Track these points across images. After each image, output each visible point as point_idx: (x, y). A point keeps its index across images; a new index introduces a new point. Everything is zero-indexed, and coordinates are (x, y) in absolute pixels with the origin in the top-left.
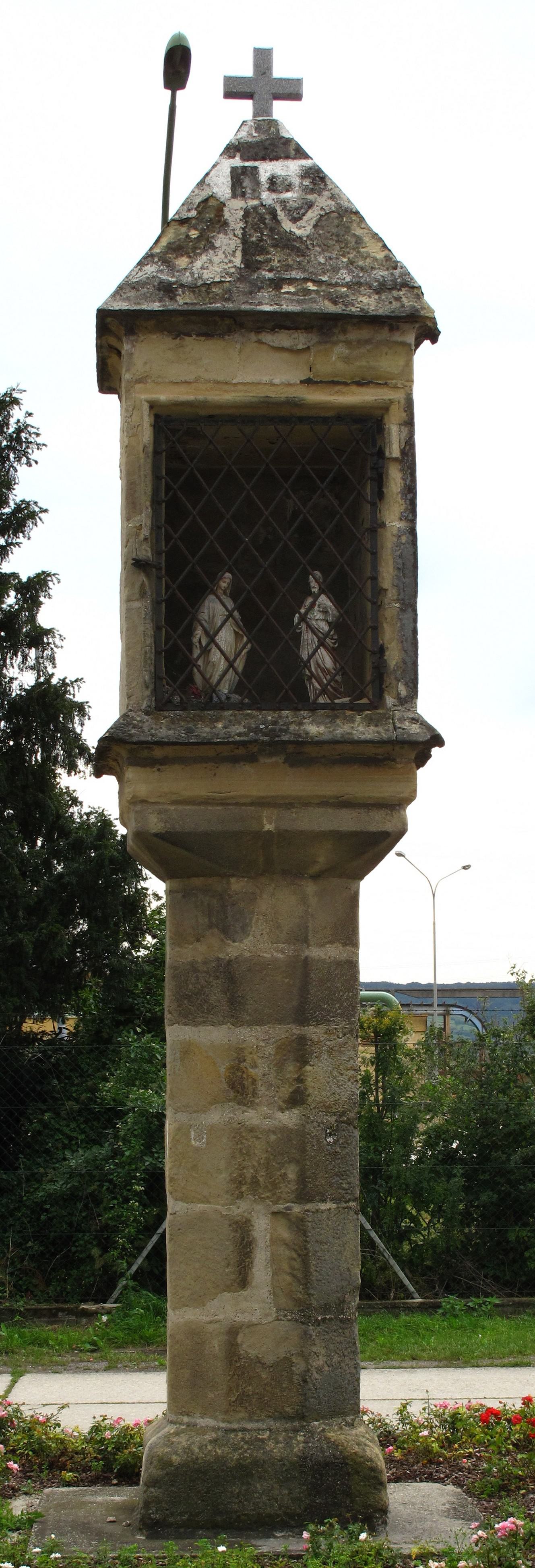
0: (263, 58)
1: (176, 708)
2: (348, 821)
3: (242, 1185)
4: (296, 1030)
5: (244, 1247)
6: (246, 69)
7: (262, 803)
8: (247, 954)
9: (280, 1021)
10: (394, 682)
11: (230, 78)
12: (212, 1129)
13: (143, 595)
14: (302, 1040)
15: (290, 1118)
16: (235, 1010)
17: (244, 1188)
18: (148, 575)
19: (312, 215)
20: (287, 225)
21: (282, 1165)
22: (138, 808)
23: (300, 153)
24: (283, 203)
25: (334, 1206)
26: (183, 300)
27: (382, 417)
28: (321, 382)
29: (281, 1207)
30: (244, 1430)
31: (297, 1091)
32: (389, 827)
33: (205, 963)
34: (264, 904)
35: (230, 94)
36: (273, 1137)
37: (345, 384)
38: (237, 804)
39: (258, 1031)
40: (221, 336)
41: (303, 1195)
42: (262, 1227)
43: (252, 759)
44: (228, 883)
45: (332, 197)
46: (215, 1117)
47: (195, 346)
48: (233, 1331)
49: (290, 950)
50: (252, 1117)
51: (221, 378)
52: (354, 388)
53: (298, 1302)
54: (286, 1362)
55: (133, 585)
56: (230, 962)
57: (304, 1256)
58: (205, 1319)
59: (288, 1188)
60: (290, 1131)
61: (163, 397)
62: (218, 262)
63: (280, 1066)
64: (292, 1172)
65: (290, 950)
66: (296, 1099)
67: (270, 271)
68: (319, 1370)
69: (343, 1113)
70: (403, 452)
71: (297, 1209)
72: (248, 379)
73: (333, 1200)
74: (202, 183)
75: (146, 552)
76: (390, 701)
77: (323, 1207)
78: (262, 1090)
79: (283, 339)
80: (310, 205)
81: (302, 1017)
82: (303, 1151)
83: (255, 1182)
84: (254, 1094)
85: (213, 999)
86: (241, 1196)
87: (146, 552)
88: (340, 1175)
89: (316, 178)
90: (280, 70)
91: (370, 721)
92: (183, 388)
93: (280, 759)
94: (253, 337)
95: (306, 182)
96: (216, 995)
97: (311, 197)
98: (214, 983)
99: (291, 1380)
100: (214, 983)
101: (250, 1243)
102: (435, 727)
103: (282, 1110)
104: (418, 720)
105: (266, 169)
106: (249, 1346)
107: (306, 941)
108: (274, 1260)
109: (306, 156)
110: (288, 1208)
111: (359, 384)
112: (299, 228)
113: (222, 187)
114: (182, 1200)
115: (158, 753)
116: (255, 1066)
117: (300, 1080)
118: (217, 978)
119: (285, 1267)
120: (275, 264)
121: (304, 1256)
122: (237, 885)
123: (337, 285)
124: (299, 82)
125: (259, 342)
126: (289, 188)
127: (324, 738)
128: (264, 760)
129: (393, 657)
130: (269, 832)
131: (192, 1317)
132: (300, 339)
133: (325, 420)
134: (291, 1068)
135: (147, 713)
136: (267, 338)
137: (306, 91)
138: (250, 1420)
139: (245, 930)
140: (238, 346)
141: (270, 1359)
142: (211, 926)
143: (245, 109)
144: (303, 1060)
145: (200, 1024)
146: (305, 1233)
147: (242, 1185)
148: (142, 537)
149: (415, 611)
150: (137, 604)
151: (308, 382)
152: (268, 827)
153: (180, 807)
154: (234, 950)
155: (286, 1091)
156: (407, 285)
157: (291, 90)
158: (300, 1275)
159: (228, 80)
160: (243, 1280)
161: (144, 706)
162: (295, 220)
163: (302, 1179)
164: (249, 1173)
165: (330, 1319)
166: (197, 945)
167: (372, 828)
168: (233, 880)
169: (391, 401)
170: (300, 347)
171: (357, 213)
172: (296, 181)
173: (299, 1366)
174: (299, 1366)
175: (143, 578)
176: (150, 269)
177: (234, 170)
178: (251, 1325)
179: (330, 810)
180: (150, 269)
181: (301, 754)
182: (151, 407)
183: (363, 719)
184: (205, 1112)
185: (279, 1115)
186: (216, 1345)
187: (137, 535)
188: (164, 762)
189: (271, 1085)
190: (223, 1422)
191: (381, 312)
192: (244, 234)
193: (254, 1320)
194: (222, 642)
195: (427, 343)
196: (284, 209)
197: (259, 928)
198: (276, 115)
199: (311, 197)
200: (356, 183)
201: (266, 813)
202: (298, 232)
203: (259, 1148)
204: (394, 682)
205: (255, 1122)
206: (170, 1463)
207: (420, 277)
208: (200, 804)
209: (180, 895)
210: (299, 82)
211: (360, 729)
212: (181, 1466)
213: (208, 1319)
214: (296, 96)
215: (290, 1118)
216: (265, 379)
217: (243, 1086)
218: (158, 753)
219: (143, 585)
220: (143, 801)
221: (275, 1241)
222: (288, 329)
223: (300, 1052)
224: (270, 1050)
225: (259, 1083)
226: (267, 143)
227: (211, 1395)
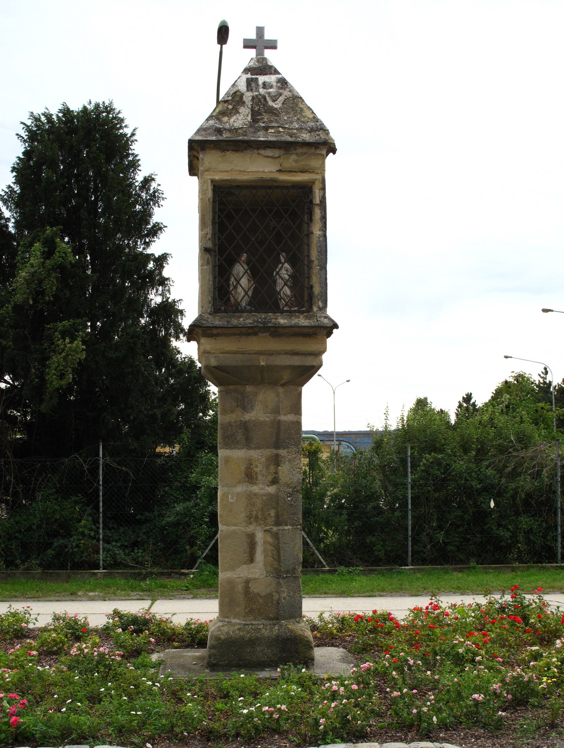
0: (260, 31)
1: (222, 312)
2: (297, 361)
3: (251, 519)
4: (275, 451)
5: (252, 545)
7: (259, 353)
8: (253, 419)
9: (267, 448)
10: (317, 301)
12: (238, 494)
13: (208, 263)
14: (277, 456)
15: (272, 490)
16: (248, 443)
20: (271, 103)
21: (268, 510)
22: (206, 355)
23: (276, 72)
24: (269, 93)
25: (291, 527)
26: (226, 136)
27: (312, 186)
30: (252, 624)
31: (275, 478)
32: (315, 363)
34: (260, 397)
35: (245, 47)
36: (264, 498)
37: (296, 172)
38: (249, 354)
39: (258, 452)
40: (242, 151)
41: (278, 523)
42: (260, 536)
43: (255, 334)
44: (245, 388)
45: (290, 91)
46: (240, 489)
48: (247, 582)
49: (272, 417)
50: (255, 489)
51: (242, 169)
52: (300, 174)
53: (275, 569)
54: (271, 594)
55: (204, 259)
56: (246, 422)
58: (235, 576)
62: (240, 119)
63: (268, 467)
64: (273, 513)
66: (275, 481)
68: (285, 599)
69: (295, 487)
70: (321, 201)
71: (275, 529)
72: (254, 170)
73: (291, 525)
74: (234, 85)
75: (210, 245)
76: (315, 309)
77: (286, 528)
78: (260, 477)
79: (269, 152)
80: (281, 95)
81: (277, 446)
82: (278, 504)
83: (257, 517)
84: (256, 479)
86: (251, 523)
87: (210, 245)
88: (293, 514)
89: (283, 83)
90: (268, 36)
91: (306, 318)
92: (225, 174)
93: (268, 334)
94: (256, 151)
95: (279, 85)
96: (240, 436)
97: (281, 91)
98: (239, 431)
99: (272, 603)
101: (255, 544)
103: (268, 486)
104: (327, 317)
105: (262, 79)
106: (255, 588)
107: (279, 413)
108: (265, 551)
109: (279, 73)
110: (271, 528)
111: (302, 172)
112: (276, 104)
114: (225, 525)
115: (215, 331)
116: (257, 467)
117: (276, 473)
118: (241, 429)
119: (270, 554)
123: (292, 129)
125: (259, 154)
126: (271, 87)
128: (261, 335)
131: (230, 576)
132: (276, 153)
133: (287, 187)
134: (272, 468)
135: (210, 314)
137: (279, 45)
138: (255, 620)
139: (252, 408)
141: (263, 594)
142: (237, 407)
143: (252, 53)
144: (278, 464)
146: (278, 539)
147: (251, 519)
150: (206, 267)
151: (280, 171)
153: (224, 355)
154: (247, 417)
155: (270, 478)
156: (323, 129)
158: (276, 557)
159: (245, 41)
160: (251, 559)
162: (274, 101)
163: (277, 516)
164: (254, 513)
165: (289, 577)
166: (232, 414)
168: (247, 386)
169: (316, 179)
170: (276, 156)
172: (275, 84)
173: (276, 597)
174: (276, 597)
175: (208, 256)
176: (211, 122)
177: (247, 79)
179: (289, 356)
180: (211, 122)
181: (276, 332)
184: (235, 487)
185: (267, 488)
186: (240, 588)
187: (206, 237)
189: (264, 475)
191: (311, 141)
193: (256, 577)
194: (243, 284)
195: (330, 159)
198: (266, 56)
199: (281, 91)
200: (300, 85)
201: (261, 357)
202: (275, 106)
205: (257, 491)
206: (220, 639)
209: (224, 393)
210: (275, 41)
211: (302, 321)
212: (225, 640)
213: (237, 576)
215: (272, 490)
216: (261, 170)
217: (252, 476)
218: (215, 331)
219: (208, 259)
220: (208, 352)
223: (276, 461)
224: (263, 460)
225: (259, 474)
226: (262, 68)
227: (238, 609)
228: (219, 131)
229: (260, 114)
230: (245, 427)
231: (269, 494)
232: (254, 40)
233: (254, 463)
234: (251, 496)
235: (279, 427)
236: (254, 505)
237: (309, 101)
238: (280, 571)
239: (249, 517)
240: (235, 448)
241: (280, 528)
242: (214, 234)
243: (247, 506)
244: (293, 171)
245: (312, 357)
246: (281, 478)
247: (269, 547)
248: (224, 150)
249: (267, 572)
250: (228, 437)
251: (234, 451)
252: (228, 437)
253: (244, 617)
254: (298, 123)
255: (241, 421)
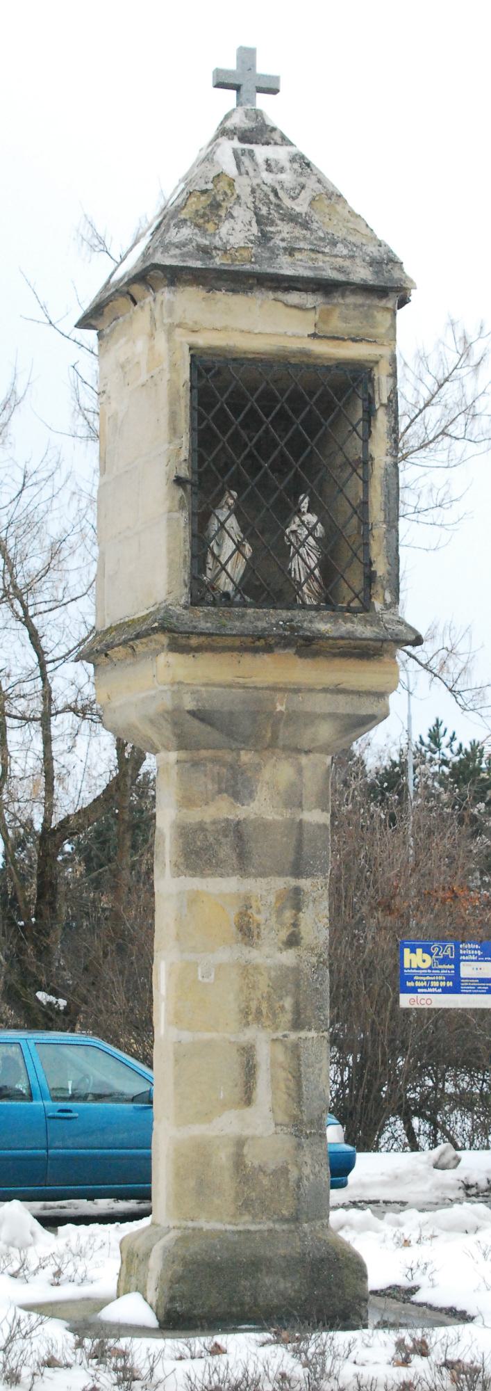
0: (247, 56)
1: (208, 604)
2: (344, 706)
3: (249, 1015)
4: (293, 882)
5: (250, 1070)
6: (230, 64)
7: (274, 689)
8: (253, 817)
9: (280, 874)
10: (380, 590)
11: (222, 71)
12: (220, 967)
13: (182, 507)
14: (297, 891)
15: (288, 958)
16: (243, 862)
17: (250, 1018)
18: (185, 490)
19: (306, 196)
20: (287, 202)
21: (281, 998)
22: (176, 687)
23: (285, 141)
24: (280, 182)
26: (218, 261)
27: (372, 369)
28: (325, 337)
29: (279, 1034)
33: (214, 823)
34: (267, 774)
35: (219, 85)
36: (273, 974)
37: (343, 340)
38: (255, 688)
39: (262, 881)
40: (245, 292)
41: (297, 1025)
42: (264, 1054)
43: (268, 649)
44: (239, 755)
45: (319, 181)
47: (223, 299)
48: (240, 1143)
49: (287, 814)
51: (245, 328)
52: (350, 343)
53: (295, 1118)
54: (284, 1171)
55: (173, 498)
56: (239, 823)
57: (298, 1079)
59: (287, 1017)
60: (288, 968)
61: (202, 340)
62: (236, 232)
63: (280, 912)
64: (288, 1003)
65: (287, 814)
66: (293, 941)
67: (283, 240)
70: (389, 400)
71: (293, 1036)
72: (268, 330)
75: (184, 472)
76: (378, 605)
78: (264, 932)
79: (294, 298)
82: (298, 986)
83: (259, 1012)
85: (222, 855)
86: (247, 1024)
87: (184, 472)
89: (303, 164)
90: (264, 67)
91: (366, 622)
92: (215, 334)
93: (291, 651)
94: (271, 295)
95: (296, 166)
96: (226, 851)
97: (302, 180)
98: (223, 840)
99: (287, 1186)
100: (223, 840)
101: (254, 1066)
102: (417, 628)
104: (401, 622)
105: (261, 152)
106: (253, 1157)
107: (300, 806)
108: (273, 1079)
110: (285, 1036)
111: (354, 340)
112: (298, 205)
113: (228, 165)
115: (194, 641)
116: (259, 912)
117: (295, 925)
119: (282, 1086)
120: (285, 235)
121: (298, 1079)
122: (246, 757)
123: (336, 256)
124: (277, 79)
126: (282, 170)
127: (331, 634)
129: (380, 568)
130: (281, 712)
132: (309, 299)
134: (288, 914)
135: (185, 608)
136: (280, 295)
138: (253, 1222)
139: (251, 796)
140: (259, 302)
141: (272, 1167)
142: (220, 792)
143: (228, 98)
144: (298, 907)
145: (209, 875)
146: (298, 1058)
147: (249, 1015)
148: (182, 458)
149: (397, 531)
150: (176, 515)
151: (314, 336)
152: (280, 708)
153: (210, 689)
154: (243, 812)
155: (284, 934)
156: (393, 261)
157: (272, 86)
158: (294, 1094)
159: (218, 72)
160: (248, 1099)
161: (182, 602)
162: (293, 198)
163: (297, 1011)
164: (253, 1005)
167: (363, 712)
168: (242, 753)
169: (381, 356)
170: (309, 306)
171: (340, 196)
172: (287, 165)
173: (294, 1174)
174: (294, 1174)
175: (181, 492)
177: (235, 152)
178: (253, 1138)
179: (329, 696)
182: (190, 349)
183: (360, 620)
185: (278, 955)
186: (223, 1157)
187: (178, 455)
188: (198, 649)
189: (272, 929)
190: (230, 1223)
191: (376, 283)
192: (255, 207)
193: (257, 1133)
196: (282, 188)
197: (262, 794)
198: (259, 106)
199: (302, 180)
200: (335, 168)
201: (279, 695)
202: (298, 209)
203: (263, 984)
204: (380, 590)
205: (259, 961)
207: (400, 254)
208: (224, 687)
209: (188, 765)
210: (277, 79)
211: (361, 630)
214: (274, 91)
215: (288, 958)
216: (281, 330)
217: (250, 930)
219: (181, 498)
220: (180, 683)
221: (274, 1063)
222: (299, 290)
225: (262, 927)
226: (258, 132)
228: (205, 251)
229: (272, 223)
230: (238, 833)
231: (281, 967)
232: (233, 72)
233: (254, 904)
234: (247, 970)
235: (301, 834)
236: (253, 987)
237: (356, 202)
238: (302, 1122)
239: (245, 1013)
240: (213, 875)
241: (303, 1034)
242: (192, 451)
243: (241, 990)
244: (338, 338)
245: (372, 699)
246: (303, 934)
247: (282, 1074)
248: (211, 289)
249: (276, 1125)
250: (197, 853)
251: (209, 879)
252: (197, 853)
253: (234, 1216)
254: (346, 246)
255: (227, 820)
